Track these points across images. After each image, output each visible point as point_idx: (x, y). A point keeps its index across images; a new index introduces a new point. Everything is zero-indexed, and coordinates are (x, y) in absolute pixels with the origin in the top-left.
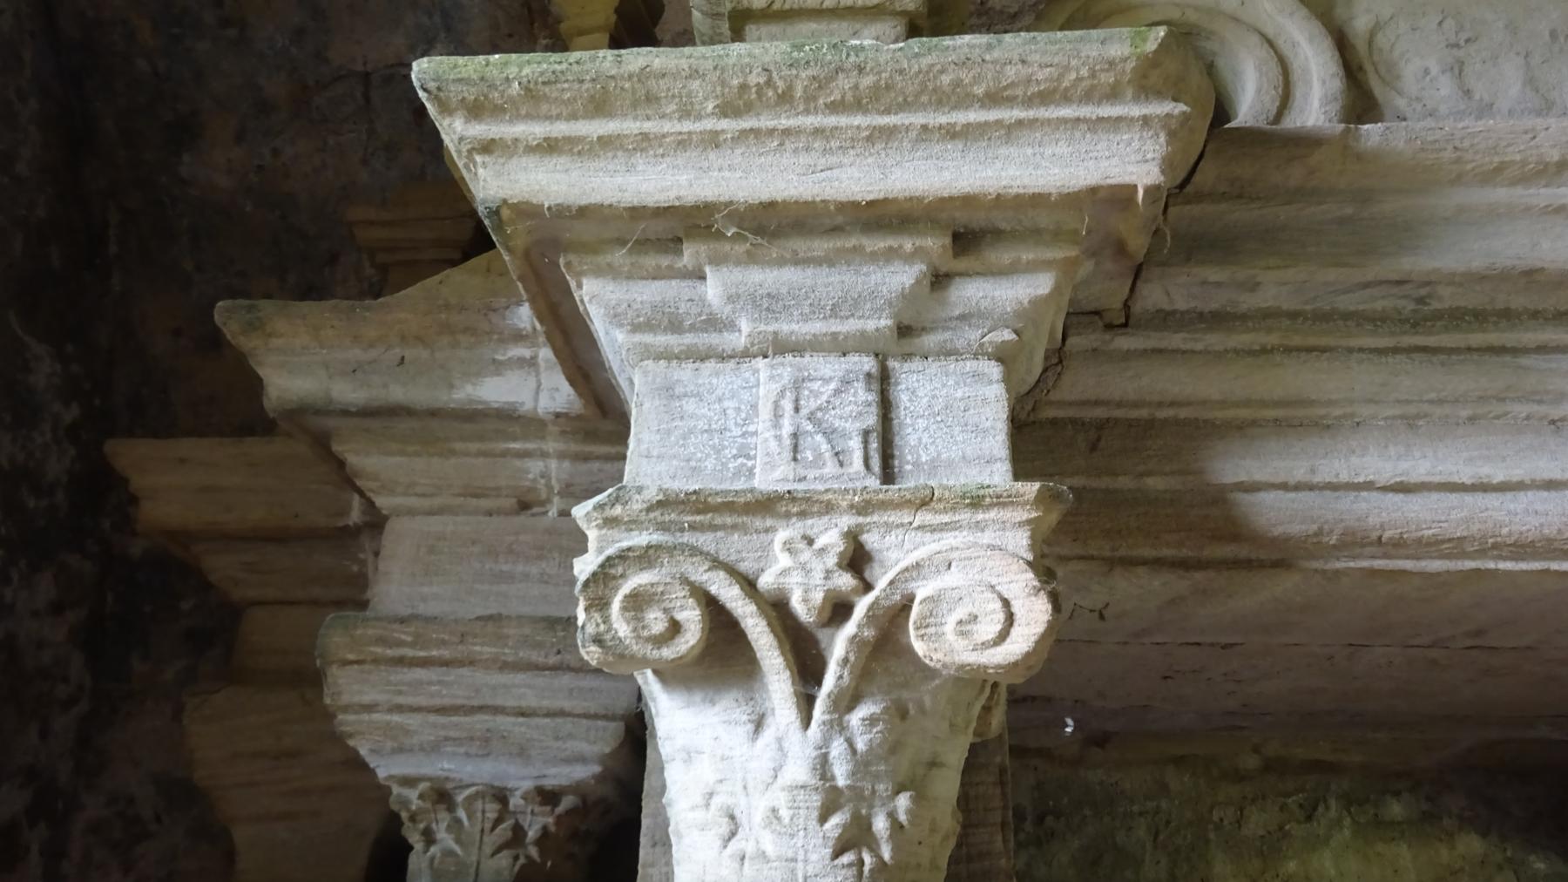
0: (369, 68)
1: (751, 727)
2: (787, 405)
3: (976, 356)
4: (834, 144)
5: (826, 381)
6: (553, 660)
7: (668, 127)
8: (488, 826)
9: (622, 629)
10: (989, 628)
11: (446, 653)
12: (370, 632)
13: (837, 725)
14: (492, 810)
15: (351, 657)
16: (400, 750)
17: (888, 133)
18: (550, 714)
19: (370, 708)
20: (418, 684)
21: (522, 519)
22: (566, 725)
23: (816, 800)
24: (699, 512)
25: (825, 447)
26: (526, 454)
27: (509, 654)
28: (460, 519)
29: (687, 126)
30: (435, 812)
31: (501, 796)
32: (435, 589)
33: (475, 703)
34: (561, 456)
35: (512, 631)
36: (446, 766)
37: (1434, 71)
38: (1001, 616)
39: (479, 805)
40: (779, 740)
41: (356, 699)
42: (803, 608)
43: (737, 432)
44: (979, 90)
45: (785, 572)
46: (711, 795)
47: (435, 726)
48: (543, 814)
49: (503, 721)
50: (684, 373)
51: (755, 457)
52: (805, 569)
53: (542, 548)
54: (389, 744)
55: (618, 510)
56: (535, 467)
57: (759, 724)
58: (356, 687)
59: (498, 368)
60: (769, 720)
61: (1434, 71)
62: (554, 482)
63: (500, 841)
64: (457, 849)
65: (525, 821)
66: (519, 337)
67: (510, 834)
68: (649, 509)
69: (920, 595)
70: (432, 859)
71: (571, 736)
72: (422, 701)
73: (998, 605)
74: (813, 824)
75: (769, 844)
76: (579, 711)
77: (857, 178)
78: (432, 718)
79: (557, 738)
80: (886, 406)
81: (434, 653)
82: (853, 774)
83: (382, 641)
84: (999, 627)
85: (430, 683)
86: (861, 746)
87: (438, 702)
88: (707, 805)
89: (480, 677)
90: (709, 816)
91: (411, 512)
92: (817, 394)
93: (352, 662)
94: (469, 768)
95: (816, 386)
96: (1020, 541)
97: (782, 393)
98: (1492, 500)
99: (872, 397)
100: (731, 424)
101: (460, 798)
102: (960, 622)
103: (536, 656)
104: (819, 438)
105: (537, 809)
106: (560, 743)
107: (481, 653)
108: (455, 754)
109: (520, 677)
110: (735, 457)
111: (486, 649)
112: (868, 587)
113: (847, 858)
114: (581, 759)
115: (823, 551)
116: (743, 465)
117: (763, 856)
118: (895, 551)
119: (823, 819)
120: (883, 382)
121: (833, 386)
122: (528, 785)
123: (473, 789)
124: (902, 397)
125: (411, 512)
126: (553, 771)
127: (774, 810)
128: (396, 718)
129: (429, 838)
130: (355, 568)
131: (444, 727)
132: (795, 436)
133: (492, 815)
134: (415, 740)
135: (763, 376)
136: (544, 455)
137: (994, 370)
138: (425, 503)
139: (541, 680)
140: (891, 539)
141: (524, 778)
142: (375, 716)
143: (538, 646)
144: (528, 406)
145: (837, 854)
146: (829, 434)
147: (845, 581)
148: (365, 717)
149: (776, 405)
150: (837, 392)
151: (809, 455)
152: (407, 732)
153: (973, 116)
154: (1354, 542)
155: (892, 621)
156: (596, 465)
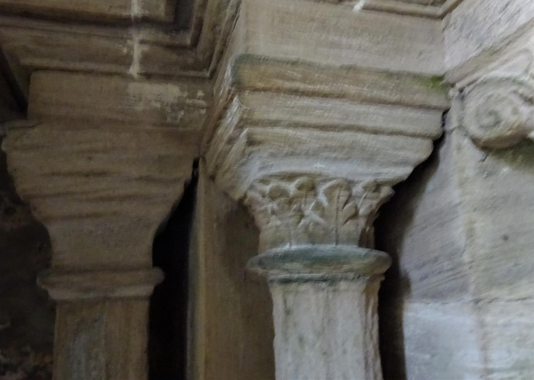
6: (395, 98)
8: (341, 205)
11: (325, 88)
16: (292, 154)
19: (275, 123)
20: (306, 110)
22: (400, 140)
27: (366, 91)
30: (306, 196)
33: (347, 123)
39: (337, 192)
41: (266, 116)
47: (318, 138)
48: (372, 198)
49: (362, 137)
54: (286, 149)
63: (349, 215)
64: (321, 220)
65: (359, 202)
70: (306, 227)
71: (402, 148)
72: (313, 120)
78: (316, 133)
79: (395, 149)
85: (315, 108)
91: (46, 69)
101: (322, 189)
105: (370, 194)
108: (327, 158)
109: (372, 109)
114: (404, 163)
122: (368, 179)
125: (46, 69)
126: (385, 170)
128: (291, 132)
130: (125, 50)
133: (343, 199)
139: (385, 111)
141: (368, 175)
142: (277, 130)
143: (384, 88)
148: (269, 130)
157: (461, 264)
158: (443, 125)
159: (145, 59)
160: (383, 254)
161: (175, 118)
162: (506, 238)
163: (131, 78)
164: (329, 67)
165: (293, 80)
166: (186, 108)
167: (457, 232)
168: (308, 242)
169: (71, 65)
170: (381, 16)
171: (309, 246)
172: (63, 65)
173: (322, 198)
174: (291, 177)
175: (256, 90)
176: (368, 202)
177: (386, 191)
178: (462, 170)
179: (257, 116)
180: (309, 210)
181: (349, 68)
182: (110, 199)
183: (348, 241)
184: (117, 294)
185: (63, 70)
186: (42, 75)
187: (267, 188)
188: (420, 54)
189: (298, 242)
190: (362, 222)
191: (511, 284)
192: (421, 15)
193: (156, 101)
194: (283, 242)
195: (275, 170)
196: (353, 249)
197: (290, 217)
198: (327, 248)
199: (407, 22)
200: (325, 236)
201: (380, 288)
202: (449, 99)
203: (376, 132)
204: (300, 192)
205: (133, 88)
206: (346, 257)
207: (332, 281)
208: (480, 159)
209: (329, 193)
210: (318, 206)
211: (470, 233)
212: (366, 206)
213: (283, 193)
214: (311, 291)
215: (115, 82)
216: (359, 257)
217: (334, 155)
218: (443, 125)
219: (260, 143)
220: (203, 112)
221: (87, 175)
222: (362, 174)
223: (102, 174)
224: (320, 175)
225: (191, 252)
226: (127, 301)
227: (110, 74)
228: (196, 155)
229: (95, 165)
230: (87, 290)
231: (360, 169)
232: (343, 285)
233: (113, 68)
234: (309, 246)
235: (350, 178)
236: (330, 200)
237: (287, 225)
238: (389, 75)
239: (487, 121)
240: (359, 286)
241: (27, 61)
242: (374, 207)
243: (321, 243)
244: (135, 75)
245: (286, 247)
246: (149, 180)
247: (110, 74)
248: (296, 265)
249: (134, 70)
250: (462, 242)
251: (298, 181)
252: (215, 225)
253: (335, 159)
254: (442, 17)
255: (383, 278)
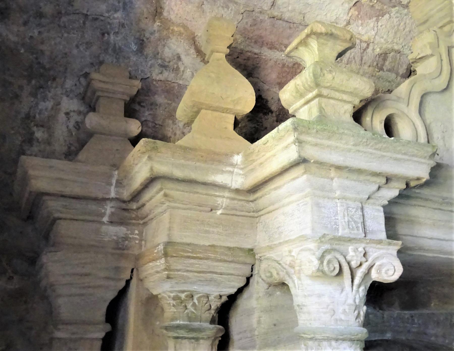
0: (89, 13)
1: (340, 291)
2: (346, 214)
3: (378, 205)
4: (373, 156)
5: (353, 208)
6: (230, 260)
7: (342, 145)
9: (326, 269)
10: (391, 272)
12: (179, 247)
13: (358, 291)
14: (205, 300)
15: (174, 255)
17: (383, 156)
18: (228, 274)
20: (192, 264)
21: (210, 214)
23: (354, 308)
24: (338, 241)
25: (354, 225)
26: (219, 196)
28: (192, 212)
29: (345, 146)
31: (208, 297)
32: (187, 234)
33: (209, 270)
34: (227, 198)
35: (218, 250)
36: (195, 288)
37: (440, 138)
38: (394, 270)
40: (347, 294)
41: (176, 268)
42: (354, 264)
43: (334, 218)
44: (403, 152)
45: (353, 256)
46: (328, 306)
48: (217, 302)
49: (215, 275)
50: (321, 201)
51: (338, 225)
52: (357, 256)
53: (217, 224)
54: (183, 281)
55: (323, 239)
56: (220, 200)
57: (342, 290)
58: (175, 264)
59: (223, 172)
60: (344, 289)
61: (440, 138)
62: (224, 205)
63: (207, 309)
66: (232, 165)
67: (209, 307)
68: (329, 240)
69: (377, 263)
70: (188, 314)
71: (233, 281)
72: (195, 269)
73: (393, 268)
74: (353, 313)
75: (343, 317)
76: (236, 274)
77: (376, 166)
78: (196, 274)
79: (229, 281)
80: (363, 215)
81: (198, 255)
82: (359, 302)
83: (184, 251)
84: (393, 273)
85: (196, 264)
86: (361, 296)
87: (199, 270)
88: (327, 308)
89: (209, 262)
90: (328, 310)
92: (351, 211)
93: (175, 257)
94: (202, 289)
95: (351, 209)
96: (395, 253)
97: (345, 211)
98: (444, 243)
99: (361, 213)
100: (332, 216)
102: (386, 271)
103: (226, 258)
104: (353, 223)
105: (217, 300)
106: (229, 283)
107: (211, 256)
108: (199, 285)
109: (220, 264)
110: (334, 225)
111: (212, 255)
112: (367, 261)
113: (357, 320)
114: (233, 287)
115: (361, 252)
116: (336, 227)
117: (341, 320)
118: (373, 254)
119: (354, 312)
120: (362, 209)
121: (354, 210)
122: (217, 294)
123: (201, 294)
124: (365, 214)
125: (65, 219)
127: (345, 310)
128: (185, 274)
129: (186, 307)
130: (103, 211)
131: (198, 277)
132: (348, 222)
133: (205, 302)
134: (190, 280)
135: (339, 205)
136: (224, 197)
137: (382, 209)
138: (184, 206)
139: (226, 265)
140: (370, 250)
142: (179, 273)
143: (226, 255)
144: (230, 185)
145: (356, 319)
146: (355, 222)
147: (364, 259)
148: (176, 273)
149: (344, 214)
150: (355, 211)
151: (351, 227)
152: (189, 278)
153: (399, 156)
154: (421, 249)
155: (370, 268)
156: (236, 202)
157: (254, 335)
158: (252, 271)
159: (112, 214)
160: (221, 327)
161: (123, 245)
162: (275, 325)
163: (103, 223)
164: (204, 246)
165: (189, 252)
166: (129, 239)
167: (254, 320)
168: (188, 321)
169: (76, 217)
170: (229, 217)
171: (188, 323)
172: (72, 217)
173: (196, 301)
174: (183, 292)
175: (172, 257)
176: (216, 303)
177: (224, 299)
178: (258, 293)
179: (172, 267)
180: (189, 306)
181: (213, 246)
182: (89, 287)
183: (206, 321)
184: (87, 336)
185: (71, 219)
186: (62, 222)
187: (172, 295)
188: (245, 235)
189: (184, 321)
190: (213, 312)
191: (275, 346)
192: (247, 216)
193: (115, 236)
194: (176, 319)
195: (177, 289)
196: (207, 325)
197: (181, 309)
198: (196, 324)
199: (240, 219)
200: (196, 319)
201: (400, 261)
202: (255, 259)
203: (221, 274)
204: (186, 298)
205: (104, 228)
206: (204, 329)
207: (197, 339)
208: (266, 288)
209: (199, 299)
210: (194, 305)
211: (259, 322)
212: (216, 304)
213: (179, 298)
214: (188, 343)
215: (94, 225)
216: (210, 329)
217: (202, 284)
218: (252, 271)
219: (172, 278)
220: (137, 242)
221: (81, 275)
222: (213, 292)
223: (87, 275)
224: (196, 291)
225: (121, 314)
226: (92, 339)
227: (93, 221)
228: (133, 267)
229: (84, 271)
230: (73, 334)
231: (213, 289)
232: (201, 341)
233: (96, 218)
234: (188, 323)
235: (208, 293)
236: (199, 302)
237: (179, 312)
238: (229, 248)
239: (268, 274)
240: (209, 342)
241: (56, 215)
242: (218, 306)
243: (194, 321)
244: (106, 222)
245: (178, 322)
246: (108, 278)
247: (93, 221)
248: (182, 331)
249: (105, 219)
250: (255, 325)
251: (186, 293)
252: (140, 304)
253: (203, 285)
254: (257, 217)
255: (220, 339)
